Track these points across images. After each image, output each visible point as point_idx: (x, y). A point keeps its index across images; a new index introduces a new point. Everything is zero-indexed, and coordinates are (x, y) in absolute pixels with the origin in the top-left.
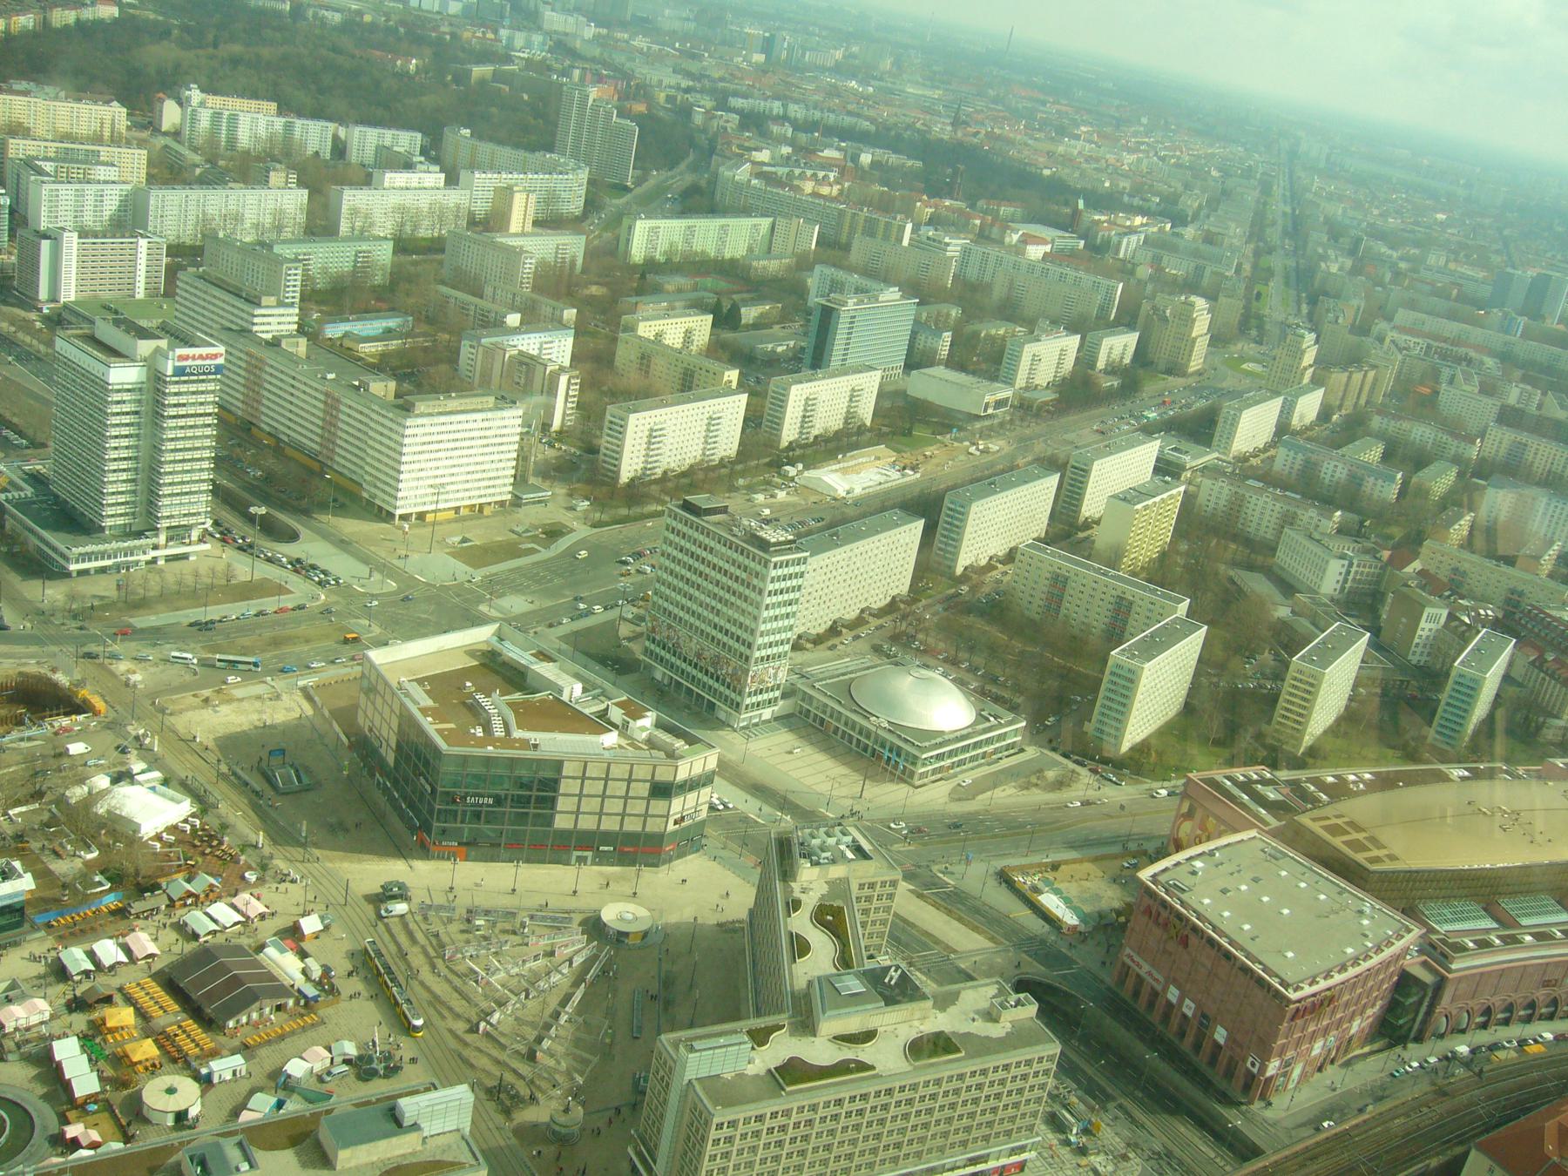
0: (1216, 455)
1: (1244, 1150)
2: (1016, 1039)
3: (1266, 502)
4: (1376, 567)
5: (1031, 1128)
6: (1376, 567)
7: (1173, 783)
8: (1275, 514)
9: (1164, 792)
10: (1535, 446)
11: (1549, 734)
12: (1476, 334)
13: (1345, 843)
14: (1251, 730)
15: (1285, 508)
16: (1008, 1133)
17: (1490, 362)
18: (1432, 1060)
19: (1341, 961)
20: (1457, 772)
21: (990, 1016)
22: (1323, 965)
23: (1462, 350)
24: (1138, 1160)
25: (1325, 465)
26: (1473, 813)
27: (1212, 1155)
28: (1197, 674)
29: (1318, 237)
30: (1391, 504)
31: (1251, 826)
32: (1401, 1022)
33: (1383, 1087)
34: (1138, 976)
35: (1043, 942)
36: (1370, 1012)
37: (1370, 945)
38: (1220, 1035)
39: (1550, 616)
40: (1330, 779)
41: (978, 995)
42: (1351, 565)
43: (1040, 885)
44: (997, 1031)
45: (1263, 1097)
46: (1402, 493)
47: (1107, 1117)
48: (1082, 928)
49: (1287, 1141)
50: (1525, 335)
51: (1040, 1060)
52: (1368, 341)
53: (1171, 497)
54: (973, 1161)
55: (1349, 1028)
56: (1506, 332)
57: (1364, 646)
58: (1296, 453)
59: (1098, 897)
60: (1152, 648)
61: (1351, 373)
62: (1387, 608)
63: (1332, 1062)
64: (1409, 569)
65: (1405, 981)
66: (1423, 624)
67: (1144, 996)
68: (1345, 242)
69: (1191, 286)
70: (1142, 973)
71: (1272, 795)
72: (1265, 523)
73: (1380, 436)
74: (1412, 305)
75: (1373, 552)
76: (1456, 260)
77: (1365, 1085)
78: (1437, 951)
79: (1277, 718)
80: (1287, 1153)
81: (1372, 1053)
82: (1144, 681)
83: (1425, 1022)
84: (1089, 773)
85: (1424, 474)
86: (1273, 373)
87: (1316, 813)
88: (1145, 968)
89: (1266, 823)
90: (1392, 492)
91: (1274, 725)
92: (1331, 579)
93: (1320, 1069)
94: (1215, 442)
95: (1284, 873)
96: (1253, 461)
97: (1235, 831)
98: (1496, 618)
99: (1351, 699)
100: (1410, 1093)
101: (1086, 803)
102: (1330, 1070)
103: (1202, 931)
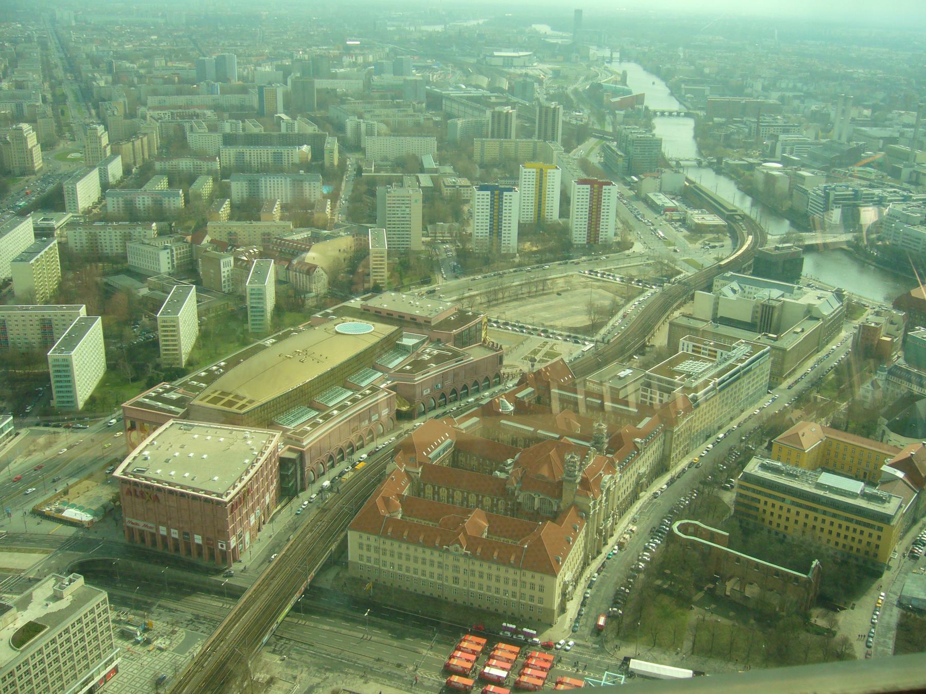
0: (71, 215)
1: (234, 593)
2: (79, 601)
3: (110, 232)
4: (186, 247)
5: (111, 646)
6: (186, 247)
7: (118, 413)
8: (118, 237)
9: (114, 421)
10: (286, 152)
11: (310, 303)
12: (197, 99)
13: (223, 405)
14: (150, 365)
15: (123, 232)
16: (99, 656)
17: (209, 113)
18: (314, 496)
19: (245, 469)
20: (269, 342)
21: (56, 597)
22: (235, 476)
23: (191, 111)
24: (182, 630)
25: (137, 199)
26: (284, 360)
27: (221, 605)
28: (107, 345)
29: (86, 67)
30: (182, 209)
31: (168, 418)
32: (290, 485)
33: (295, 523)
34: (139, 530)
35: (76, 538)
36: (272, 488)
37: (256, 453)
38: (198, 539)
39: (288, 240)
40: (203, 374)
41: (47, 587)
42: (172, 251)
43: (61, 507)
44: (64, 604)
45: (235, 560)
46: (187, 201)
47: (154, 616)
48: (96, 519)
49: (257, 576)
50: (224, 92)
51: (98, 606)
52: (136, 120)
53: (51, 249)
54: (85, 683)
55: (265, 501)
56: (212, 93)
57: (195, 293)
58: (118, 198)
59: (99, 498)
60: (71, 343)
61: (133, 142)
62: (200, 268)
63: (264, 523)
64: (205, 242)
65: (284, 463)
66: (223, 269)
67: (148, 539)
68: (103, 66)
69: (18, 117)
70: (141, 527)
71: (174, 396)
72: (114, 245)
73: (163, 173)
74: (155, 93)
75: (182, 240)
76: (171, 61)
77: (285, 526)
78: (292, 440)
79: (162, 352)
80: (258, 583)
81: (283, 508)
82: (75, 363)
83: (302, 479)
84: (64, 430)
85: (195, 186)
86: (87, 156)
87: (202, 396)
88: (141, 525)
89: (177, 413)
90: (180, 202)
91: (163, 357)
92: (164, 263)
93: (259, 530)
94: (67, 207)
95: (196, 436)
96: (95, 211)
97: (161, 424)
98: (260, 252)
99: (200, 325)
100: (308, 519)
101: (70, 447)
102: (264, 527)
103: (163, 488)
